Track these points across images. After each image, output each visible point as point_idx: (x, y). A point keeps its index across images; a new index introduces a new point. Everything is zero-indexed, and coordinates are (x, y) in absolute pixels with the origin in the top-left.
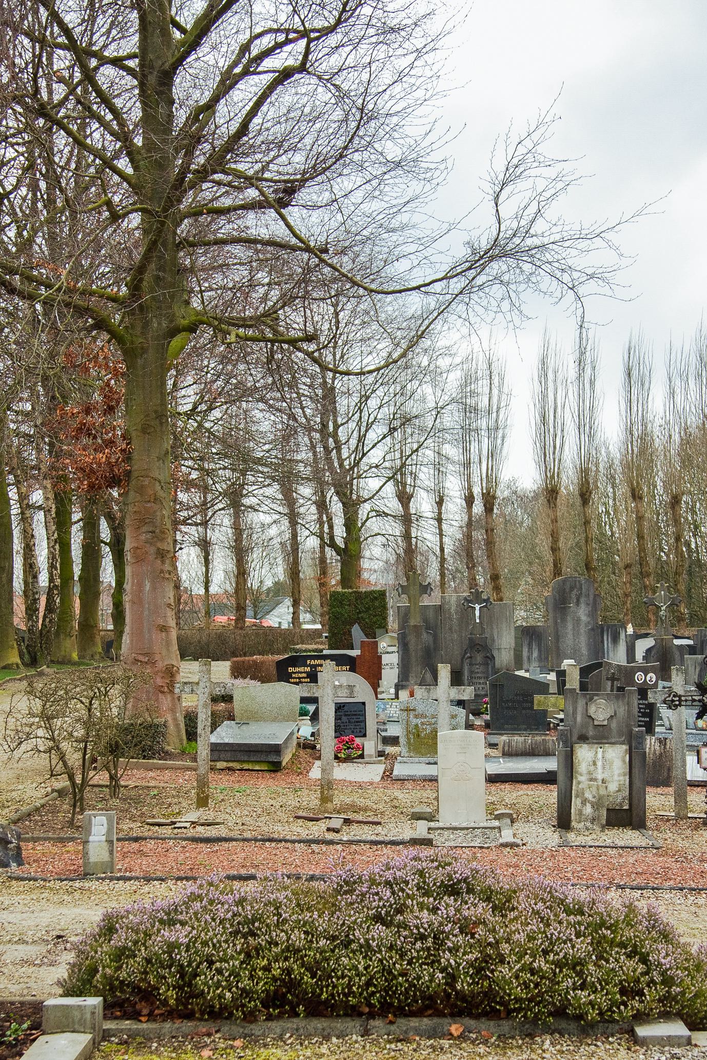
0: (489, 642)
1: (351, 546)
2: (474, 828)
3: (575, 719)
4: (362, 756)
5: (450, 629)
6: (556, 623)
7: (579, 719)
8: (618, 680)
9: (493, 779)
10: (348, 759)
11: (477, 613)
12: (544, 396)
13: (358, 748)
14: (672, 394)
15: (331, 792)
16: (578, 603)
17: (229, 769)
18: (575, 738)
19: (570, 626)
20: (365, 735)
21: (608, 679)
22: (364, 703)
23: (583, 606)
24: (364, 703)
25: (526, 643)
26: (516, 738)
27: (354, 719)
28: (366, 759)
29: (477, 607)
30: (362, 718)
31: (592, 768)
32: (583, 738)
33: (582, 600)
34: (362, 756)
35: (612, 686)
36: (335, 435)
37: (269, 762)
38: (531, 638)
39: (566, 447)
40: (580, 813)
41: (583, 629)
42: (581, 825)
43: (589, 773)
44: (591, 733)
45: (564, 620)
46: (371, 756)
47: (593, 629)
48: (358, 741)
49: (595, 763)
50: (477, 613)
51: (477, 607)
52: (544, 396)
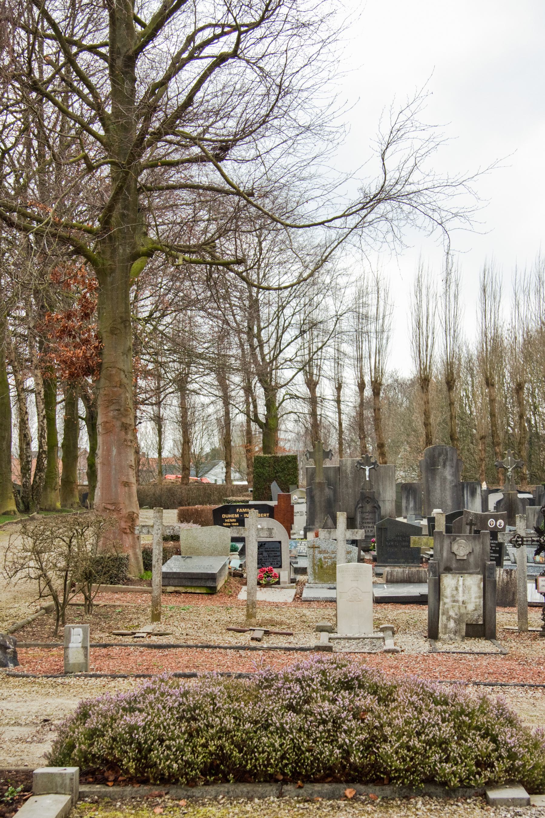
0: (376, 495)
1: (270, 422)
2: (364, 638)
3: (442, 554)
4: (278, 583)
5: (347, 485)
6: (427, 481)
7: (445, 554)
8: (475, 525)
9: (379, 601)
10: (268, 585)
11: (367, 473)
12: (419, 307)
13: (275, 576)
14: (517, 305)
15: (254, 610)
16: (444, 466)
17: (176, 592)
18: (441, 570)
19: (438, 483)
20: (280, 567)
21: (467, 524)
22: (280, 542)
23: (448, 468)
24: (280, 542)
25: (404, 496)
26: (397, 569)
27: (273, 554)
28: (282, 585)
29: (367, 468)
30: (278, 554)
31: (455, 592)
32: (448, 570)
33: (448, 463)
34: (278, 583)
35: (471, 529)
36: (259, 336)
37: (207, 587)
38: (408, 493)
39: (436, 346)
40: (446, 627)
41: (448, 486)
42: (446, 636)
43: (453, 596)
44: (454, 566)
45: (433, 479)
46: (285, 583)
47: (456, 486)
48: (275, 571)
49: (457, 589)
50: (367, 473)
51: (367, 468)
52: (419, 307)
